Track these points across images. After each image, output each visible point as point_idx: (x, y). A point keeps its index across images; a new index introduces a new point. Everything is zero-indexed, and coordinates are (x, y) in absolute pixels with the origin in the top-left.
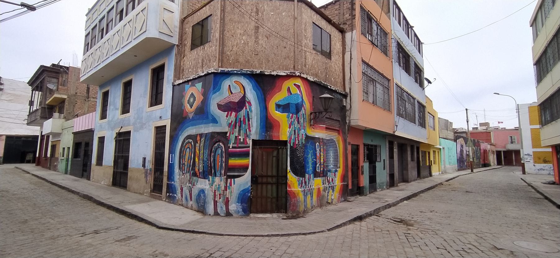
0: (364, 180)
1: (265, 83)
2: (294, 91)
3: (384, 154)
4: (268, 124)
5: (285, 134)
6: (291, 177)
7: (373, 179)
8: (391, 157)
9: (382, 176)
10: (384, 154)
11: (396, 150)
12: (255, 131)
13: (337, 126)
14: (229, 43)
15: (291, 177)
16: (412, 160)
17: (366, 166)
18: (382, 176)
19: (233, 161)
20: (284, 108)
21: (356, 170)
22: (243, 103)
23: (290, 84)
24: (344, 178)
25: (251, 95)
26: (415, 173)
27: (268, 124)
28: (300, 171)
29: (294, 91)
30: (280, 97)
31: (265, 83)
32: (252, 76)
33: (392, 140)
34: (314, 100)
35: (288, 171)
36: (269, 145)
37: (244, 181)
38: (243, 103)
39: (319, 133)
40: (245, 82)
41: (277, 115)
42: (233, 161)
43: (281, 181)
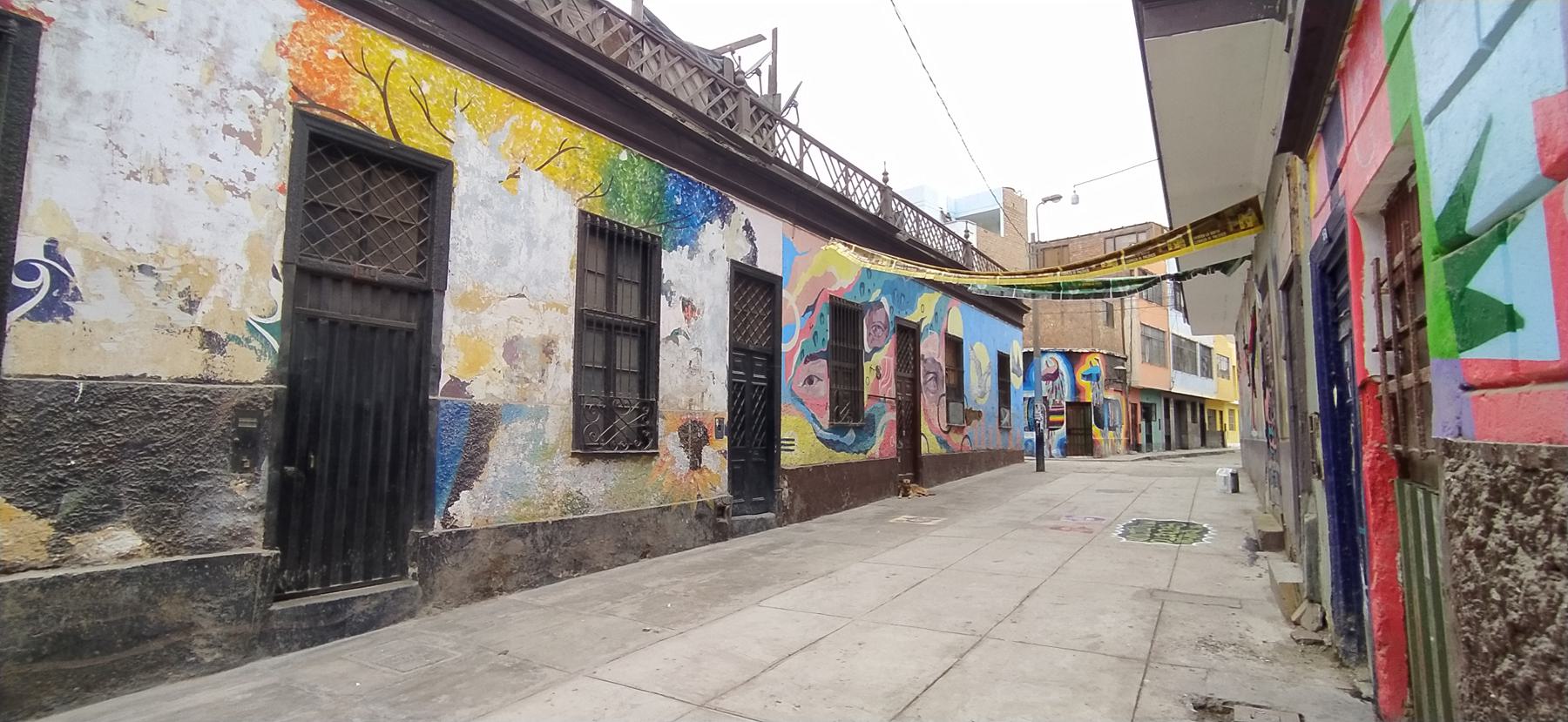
0: (1142, 439)
1: (1073, 358)
2: (1095, 363)
3: (1160, 412)
4: (1077, 390)
5: (1089, 397)
6: (1095, 428)
7: (1149, 439)
8: (1167, 416)
9: (1158, 437)
10: (1160, 412)
11: (1172, 409)
12: (1067, 396)
13: (1119, 387)
14: (1041, 331)
15: (1095, 428)
16: (1194, 421)
17: (1143, 424)
18: (1158, 437)
19: (1052, 418)
20: (1088, 377)
21: (1134, 426)
22: (1057, 374)
23: (1090, 358)
24: (1127, 433)
25: (1063, 368)
26: (1198, 440)
27: (1077, 390)
28: (1100, 425)
29: (1095, 363)
30: (1083, 369)
31: (1073, 358)
32: (1063, 353)
33: (1167, 397)
34: (1108, 367)
35: (861, 457)
36: (1078, 407)
37: (1061, 432)
38: (1057, 374)
39: (1111, 396)
40: (1058, 358)
41: (1083, 382)
42: (1052, 418)
43: (1088, 432)
